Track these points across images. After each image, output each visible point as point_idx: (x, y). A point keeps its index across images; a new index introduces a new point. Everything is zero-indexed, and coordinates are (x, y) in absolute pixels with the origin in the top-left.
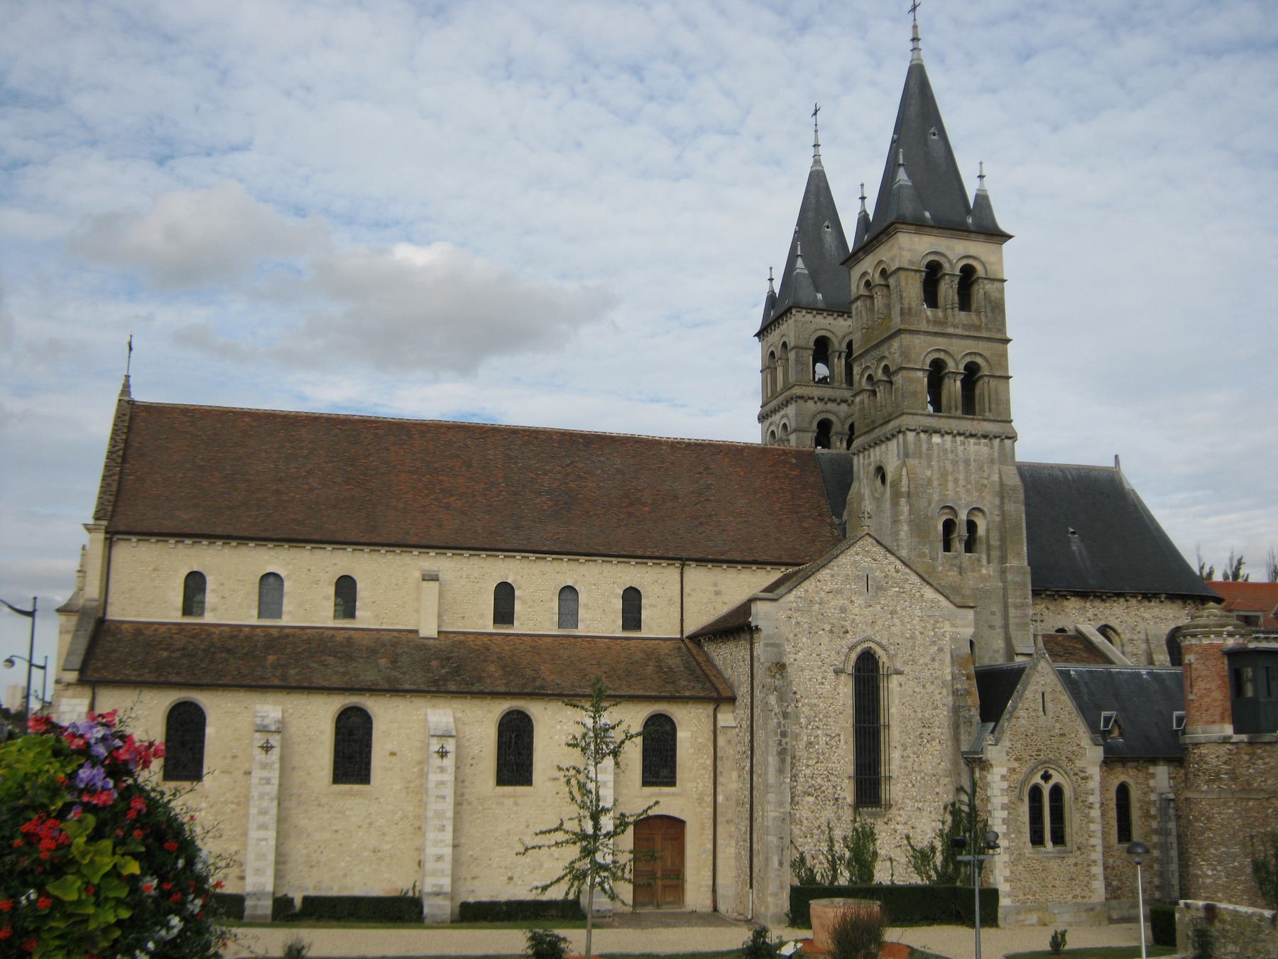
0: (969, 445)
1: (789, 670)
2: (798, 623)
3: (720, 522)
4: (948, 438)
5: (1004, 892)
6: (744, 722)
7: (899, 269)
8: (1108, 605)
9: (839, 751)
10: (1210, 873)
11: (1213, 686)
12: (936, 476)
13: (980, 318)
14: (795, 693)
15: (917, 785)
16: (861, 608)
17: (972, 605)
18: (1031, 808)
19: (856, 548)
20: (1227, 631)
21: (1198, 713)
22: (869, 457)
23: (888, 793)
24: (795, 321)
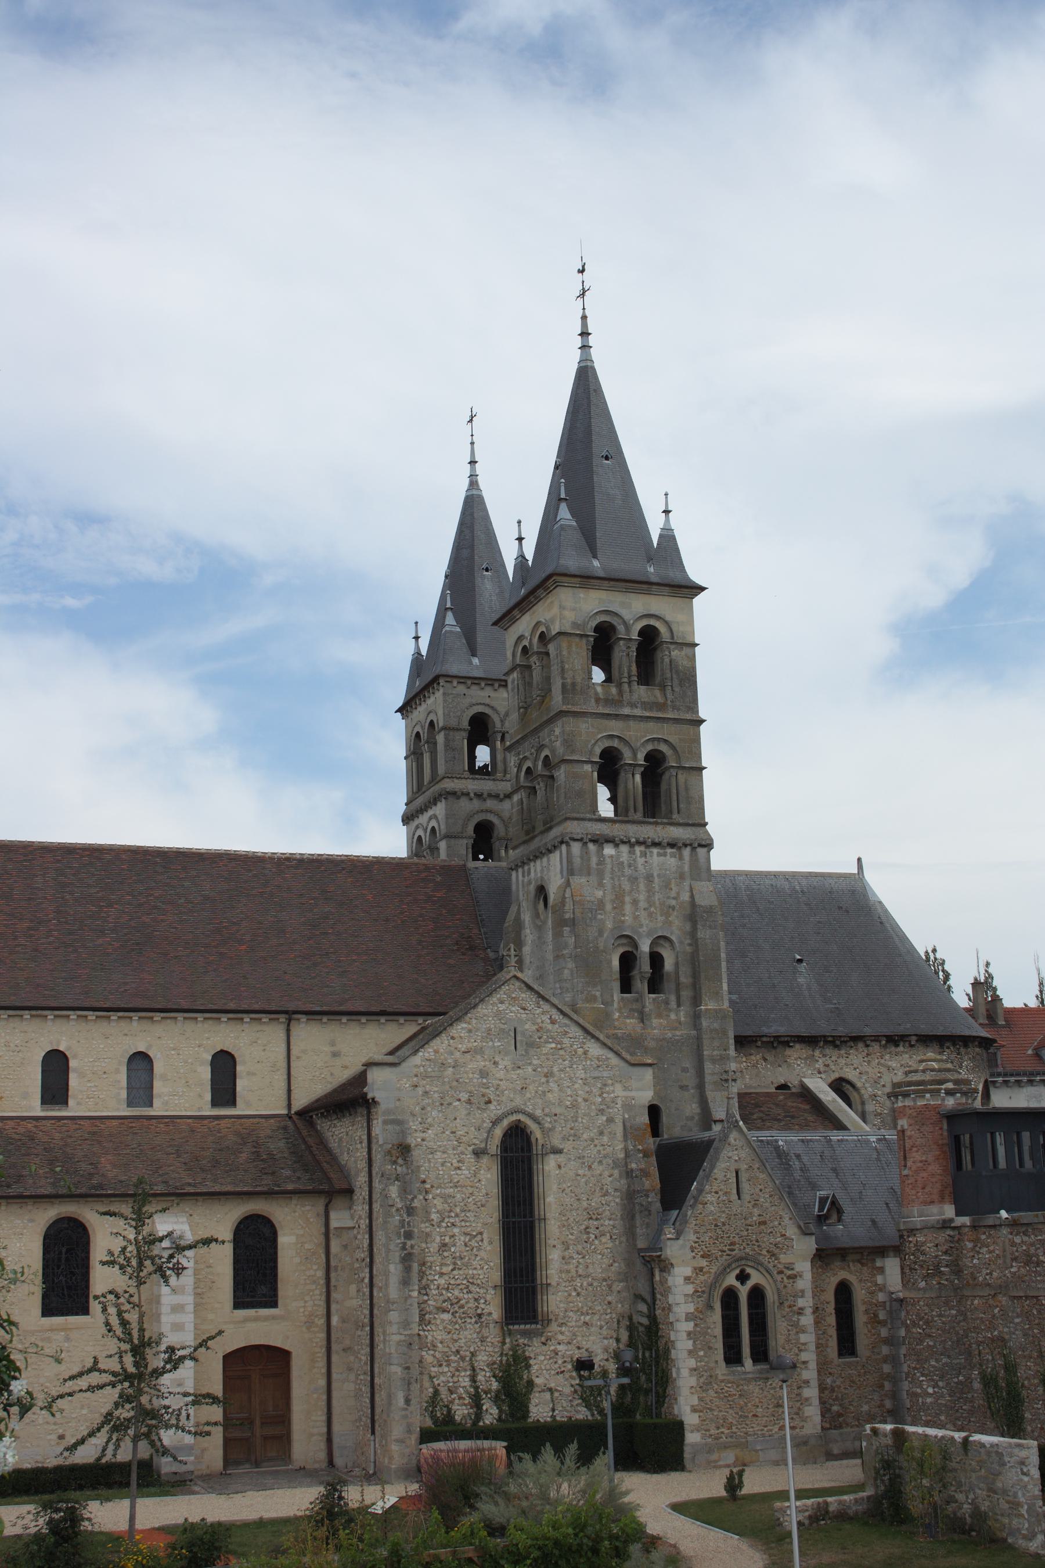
0: (651, 856)
1: (415, 1153)
2: (426, 1092)
3: (340, 961)
4: (625, 849)
5: (690, 1425)
6: (362, 1221)
7: (560, 634)
8: (843, 1052)
9: (482, 1254)
10: (930, 1390)
11: (930, 1158)
12: (609, 897)
13: (665, 695)
14: (424, 1182)
15: (583, 1292)
16: (507, 1071)
17: (649, 1061)
18: (723, 1317)
19: (501, 994)
20: (945, 1090)
21: (914, 1192)
22: (529, 873)
23: (545, 1304)
24: (444, 694)
